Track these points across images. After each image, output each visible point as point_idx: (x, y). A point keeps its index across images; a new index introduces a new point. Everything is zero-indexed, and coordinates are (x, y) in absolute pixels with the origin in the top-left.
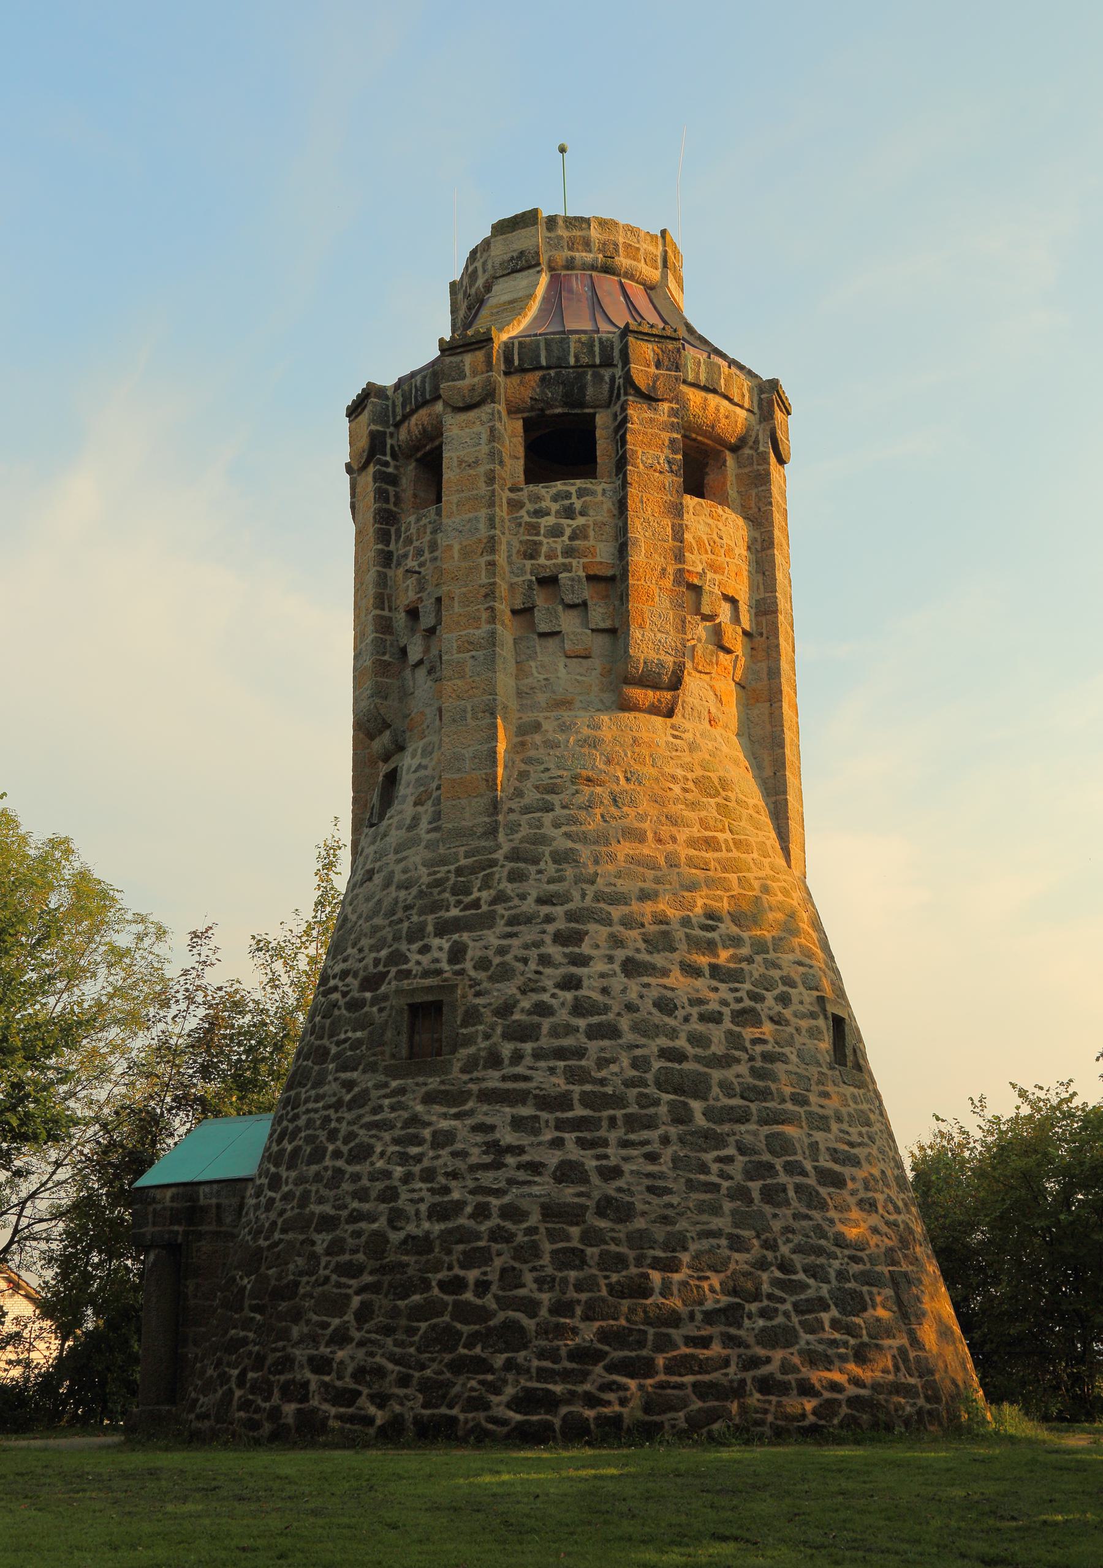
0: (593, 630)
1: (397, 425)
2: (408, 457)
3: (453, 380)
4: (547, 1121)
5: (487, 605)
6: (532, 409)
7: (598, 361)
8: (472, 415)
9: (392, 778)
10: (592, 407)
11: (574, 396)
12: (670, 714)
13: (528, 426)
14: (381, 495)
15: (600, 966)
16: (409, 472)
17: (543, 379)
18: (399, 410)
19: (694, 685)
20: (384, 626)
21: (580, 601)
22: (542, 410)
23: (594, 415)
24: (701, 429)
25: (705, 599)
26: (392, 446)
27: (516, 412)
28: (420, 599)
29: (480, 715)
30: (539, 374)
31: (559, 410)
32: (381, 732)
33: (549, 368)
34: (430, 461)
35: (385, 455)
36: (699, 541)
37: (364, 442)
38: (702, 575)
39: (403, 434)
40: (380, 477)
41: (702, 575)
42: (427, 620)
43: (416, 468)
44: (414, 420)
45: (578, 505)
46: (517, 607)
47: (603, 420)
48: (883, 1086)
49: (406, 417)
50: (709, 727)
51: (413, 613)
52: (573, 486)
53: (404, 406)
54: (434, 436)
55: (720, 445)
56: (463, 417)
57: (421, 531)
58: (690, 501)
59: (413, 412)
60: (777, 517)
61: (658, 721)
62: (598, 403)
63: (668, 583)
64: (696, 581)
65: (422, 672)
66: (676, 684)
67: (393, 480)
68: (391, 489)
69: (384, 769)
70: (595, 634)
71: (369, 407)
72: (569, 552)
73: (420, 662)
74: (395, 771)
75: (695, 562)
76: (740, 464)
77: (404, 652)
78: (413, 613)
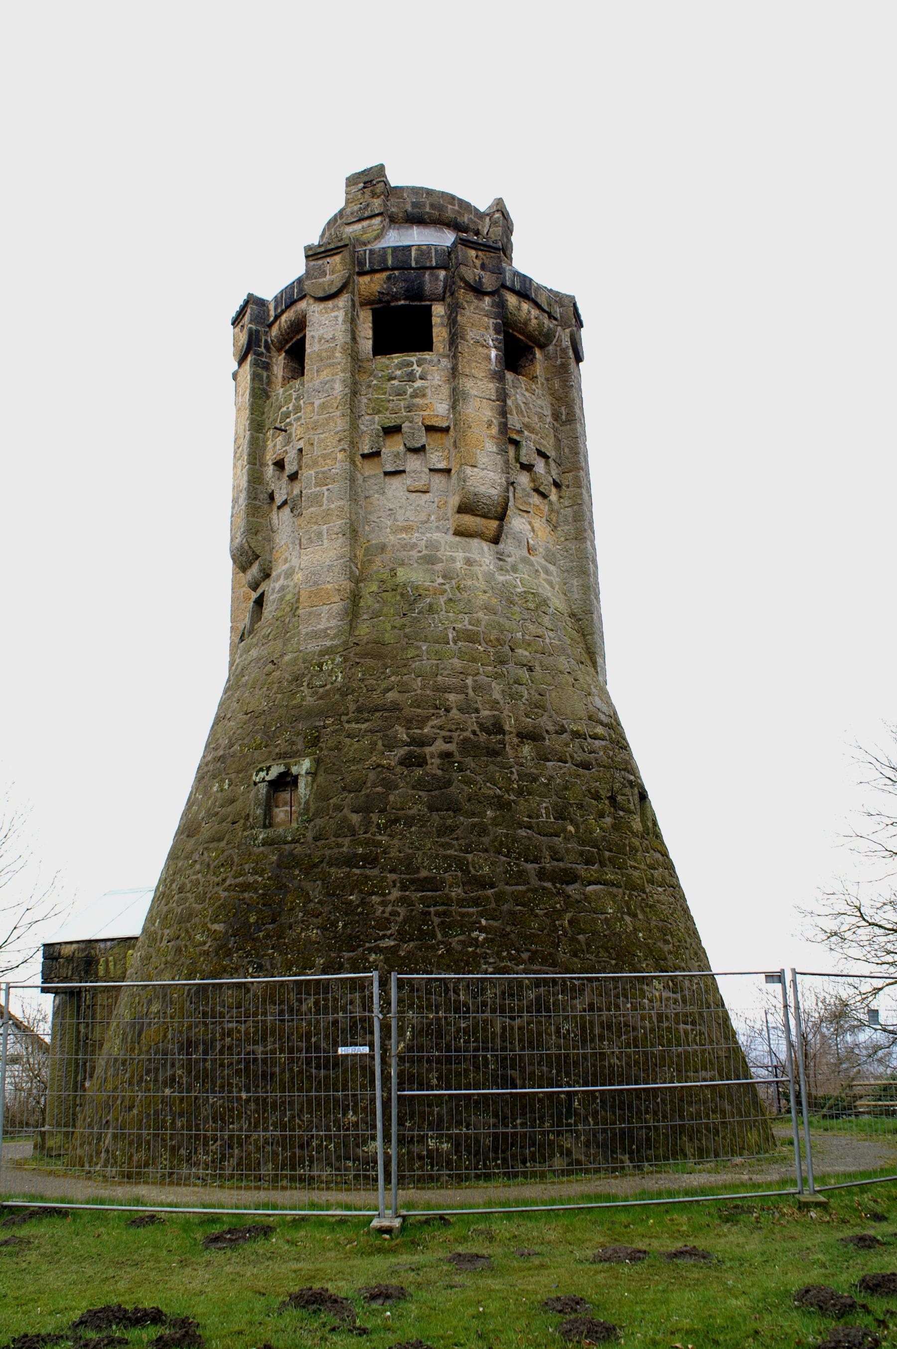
0: (431, 470)
1: (270, 326)
2: (279, 350)
3: (315, 278)
4: (394, 882)
5: (341, 447)
6: (380, 301)
7: (434, 264)
8: (330, 304)
9: (259, 602)
10: (429, 300)
11: (416, 293)
12: (496, 540)
13: (375, 313)
14: (255, 377)
15: (440, 746)
16: (279, 363)
17: (389, 278)
18: (272, 313)
19: (517, 523)
20: (255, 479)
21: (420, 445)
22: (388, 302)
23: (431, 306)
24: (516, 326)
25: (523, 451)
26: (266, 341)
27: (366, 305)
28: (286, 452)
29: (334, 536)
30: (385, 275)
31: (402, 302)
32: (251, 564)
33: (393, 269)
34: (296, 351)
35: (260, 347)
36: (517, 407)
37: (243, 338)
38: (520, 432)
39: (275, 331)
40: (255, 364)
41: (520, 432)
42: (290, 468)
43: (285, 359)
44: (284, 318)
45: (418, 371)
46: (366, 452)
47: (439, 310)
48: (674, 855)
49: (277, 317)
50: (528, 555)
51: (280, 465)
52: (413, 358)
53: (276, 308)
54: (299, 326)
55: (531, 341)
56: (322, 305)
57: (288, 400)
58: (509, 376)
59: (283, 312)
60: (577, 401)
61: (485, 546)
62: (434, 297)
63: (494, 430)
64: (515, 437)
65: (287, 510)
66: (502, 517)
67: (267, 367)
68: (265, 374)
69: (254, 595)
70: (432, 473)
71: (249, 311)
72: (409, 409)
73: (285, 503)
74: (262, 595)
75: (514, 421)
76: (547, 357)
77: (272, 497)
78: (280, 465)
